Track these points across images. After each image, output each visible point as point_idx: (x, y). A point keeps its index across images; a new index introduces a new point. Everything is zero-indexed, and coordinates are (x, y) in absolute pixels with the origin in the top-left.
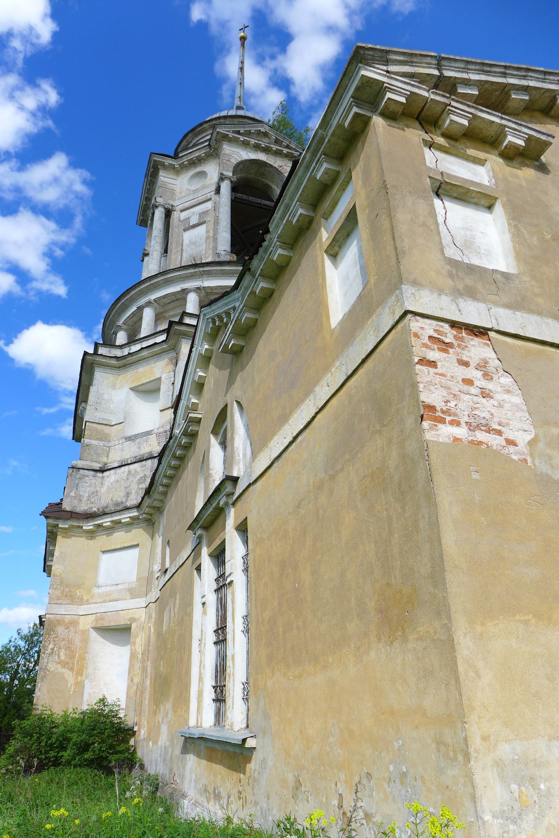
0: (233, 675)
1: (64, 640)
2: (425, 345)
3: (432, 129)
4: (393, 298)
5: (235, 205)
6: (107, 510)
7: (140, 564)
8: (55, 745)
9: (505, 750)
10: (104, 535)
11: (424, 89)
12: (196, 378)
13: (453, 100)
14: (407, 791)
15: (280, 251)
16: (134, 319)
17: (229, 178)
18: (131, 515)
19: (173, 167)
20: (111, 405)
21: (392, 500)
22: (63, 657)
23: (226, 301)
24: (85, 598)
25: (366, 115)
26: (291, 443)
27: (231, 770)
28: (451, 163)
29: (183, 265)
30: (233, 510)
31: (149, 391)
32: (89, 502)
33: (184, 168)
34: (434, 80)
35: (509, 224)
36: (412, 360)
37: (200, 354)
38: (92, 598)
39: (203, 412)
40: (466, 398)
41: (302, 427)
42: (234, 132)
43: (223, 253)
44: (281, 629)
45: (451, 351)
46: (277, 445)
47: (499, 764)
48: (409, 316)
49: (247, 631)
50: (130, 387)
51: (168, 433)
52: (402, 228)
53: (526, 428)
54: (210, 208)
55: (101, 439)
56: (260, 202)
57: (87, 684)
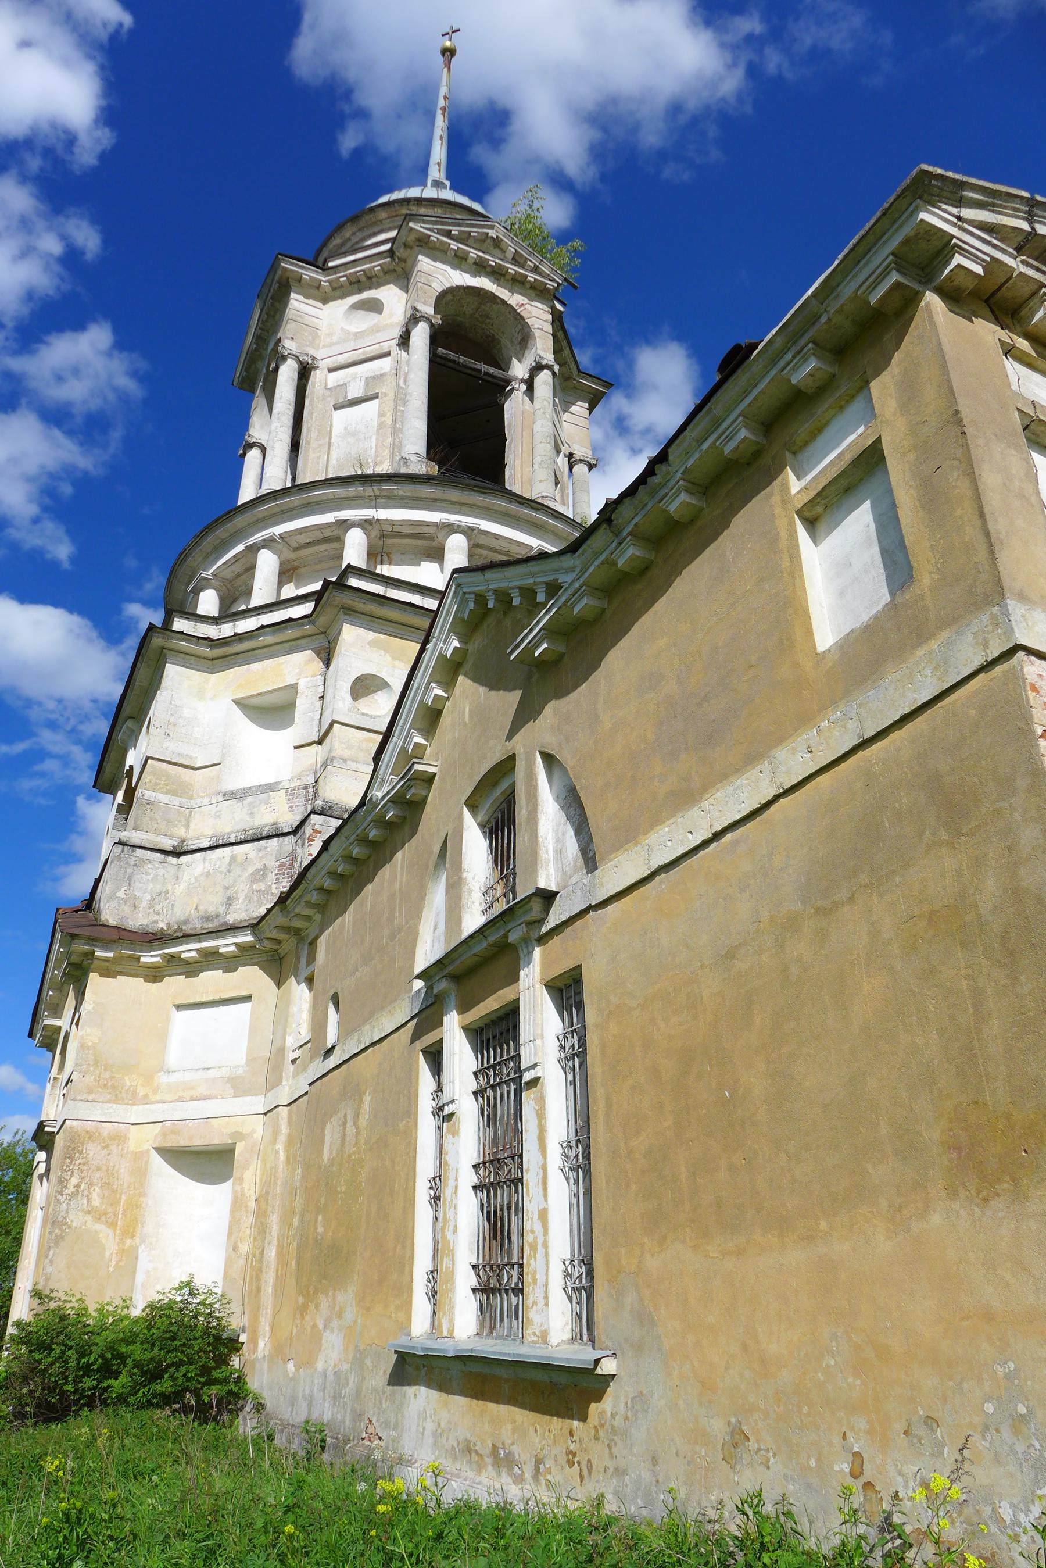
0: (545, 1245)
1: (99, 1169)
3: (1009, 321)
4: (985, 618)
6: (187, 929)
7: (253, 1031)
8: (95, 1367)
10: (180, 974)
11: (1011, 255)
12: (429, 701)
15: (683, 497)
16: (237, 568)
17: (428, 320)
18: (240, 940)
21: (984, 962)
22: (96, 1202)
23: (533, 570)
24: (141, 1091)
25: (912, 288)
26: (705, 844)
27: (544, 1413)
28: (1037, 385)
29: (330, 476)
30: (537, 949)
31: (271, 711)
32: (151, 911)
33: (338, 292)
34: (1020, 238)
36: (1032, 731)
37: (442, 657)
38: (155, 1092)
39: (438, 763)
41: (738, 817)
42: (440, 232)
43: (413, 458)
44: (683, 1169)
46: (669, 844)
48: (1021, 654)
49: (582, 1164)
50: (235, 697)
51: (311, 790)
52: (993, 500)
54: (387, 369)
55: (174, 793)
56: (478, 367)
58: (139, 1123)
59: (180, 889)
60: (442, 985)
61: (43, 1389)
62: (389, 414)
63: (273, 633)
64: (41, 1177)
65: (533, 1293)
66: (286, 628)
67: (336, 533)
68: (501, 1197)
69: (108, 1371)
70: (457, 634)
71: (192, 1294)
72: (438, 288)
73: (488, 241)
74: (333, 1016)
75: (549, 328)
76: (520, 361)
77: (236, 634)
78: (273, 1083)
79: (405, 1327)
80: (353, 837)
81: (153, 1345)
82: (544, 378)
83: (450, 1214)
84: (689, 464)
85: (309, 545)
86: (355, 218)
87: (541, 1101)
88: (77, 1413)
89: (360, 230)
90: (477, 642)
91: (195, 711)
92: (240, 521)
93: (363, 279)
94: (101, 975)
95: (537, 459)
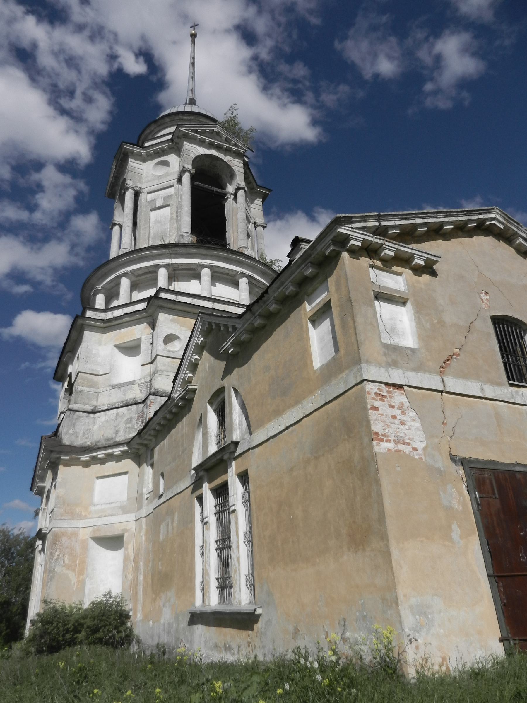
0: (239, 570)
1: (67, 548)
2: (373, 399)
5: (195, 191)
6: (100, 445)
9: (413, 601)
13: (386, 241)
14: (367, 624)
15: (274, 306)
16: (112, 284)
17: (189, 171)
19: (140, 155)
20: (99, 358)
22: (67, 561)
24: (83, 514)
26: (284, 430)
31: (131, 349)
35: (415, 316)
40: (393, 426)
41: (293, 422)
42: (193, 131)
43: (186, 235)
45: (385, 400)
47: (411, 607)
48: (365, 382)
49: (250, 542)
51: (149, 384)
53: (422, 440)
55: (90, 386)
57: (87, 582)
58: (84, 527)
59: (96, 427)
60: (201, 473)
61: (50, 640)
62: (175, 214)
63: (130, 317)
64: (40, 552)
65: (235, 588)
66: (135, 315)
67: (154, 269)
68: (225, 553)
69: (77, 630)
70: (202, 336)
71: (111, 597)
72: (193, 156)
73: (214, 133)
74: (162, 481)
75: (242, 170)
76: (230, 185)
77: (114, 317)
78: (138, 508)
79: (193, 604)
80: (166, 411)
81: (94, 619)
82: (241, 193)
83: (207, 560)
84: (275, 295)
85: (143, 274)
86: (155, 121)
87: (236, 518)
88: (64, 648)
89: (158, 126)
90: (210, 339)
91: (98, 351)
92: (112, 265)
93: (160, 152)
94: (64, 466)
95: (240, 230)
